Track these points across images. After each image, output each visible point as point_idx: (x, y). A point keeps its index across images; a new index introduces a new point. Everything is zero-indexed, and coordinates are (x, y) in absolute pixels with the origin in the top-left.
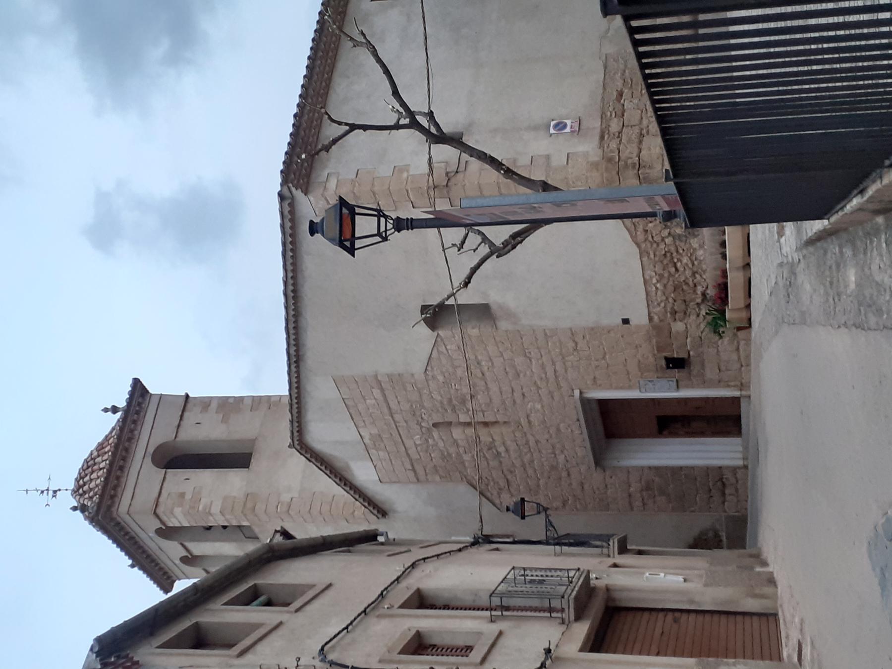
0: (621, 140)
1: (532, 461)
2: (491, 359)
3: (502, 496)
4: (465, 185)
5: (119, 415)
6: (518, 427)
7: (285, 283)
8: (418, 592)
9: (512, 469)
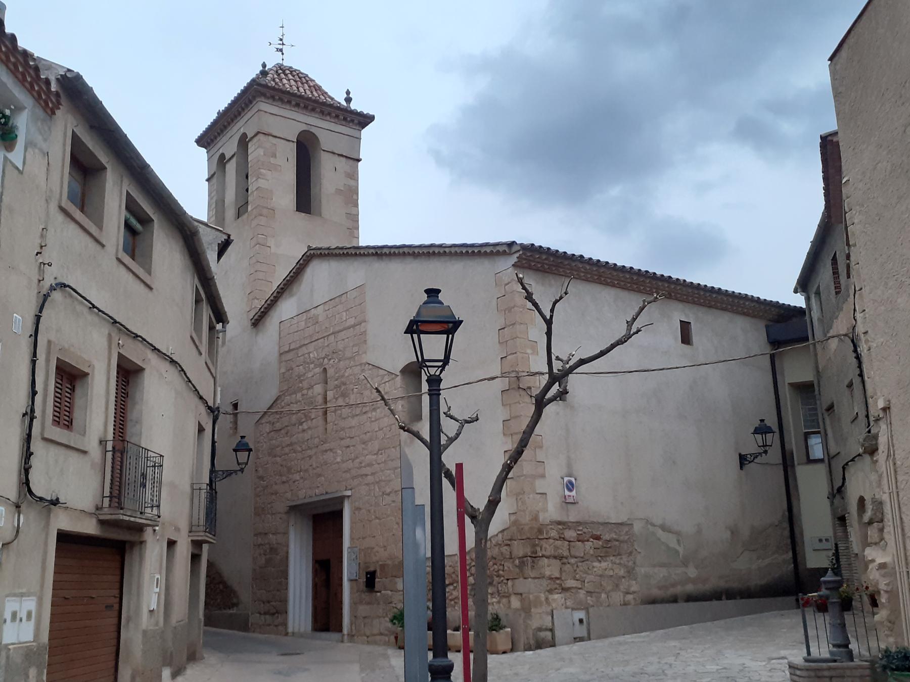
0: (557, 540)
1: (295, 452)
2: (376, 420)
3: (268, 424)
4: (520, 404)
5: (344, 103)
6: (322, 441)
7: (440, 246)
8: (139, 370)
9: (289, 434)
